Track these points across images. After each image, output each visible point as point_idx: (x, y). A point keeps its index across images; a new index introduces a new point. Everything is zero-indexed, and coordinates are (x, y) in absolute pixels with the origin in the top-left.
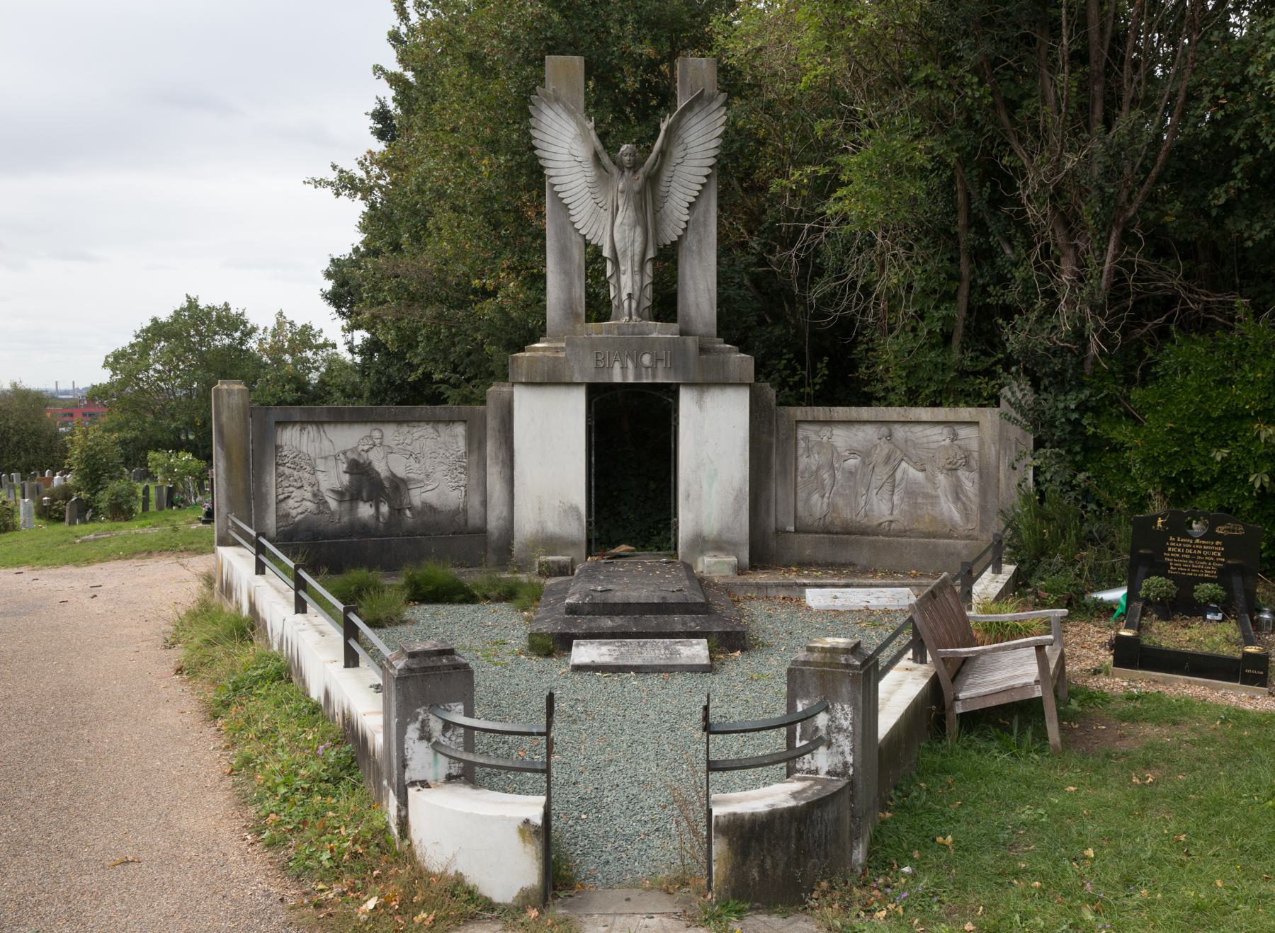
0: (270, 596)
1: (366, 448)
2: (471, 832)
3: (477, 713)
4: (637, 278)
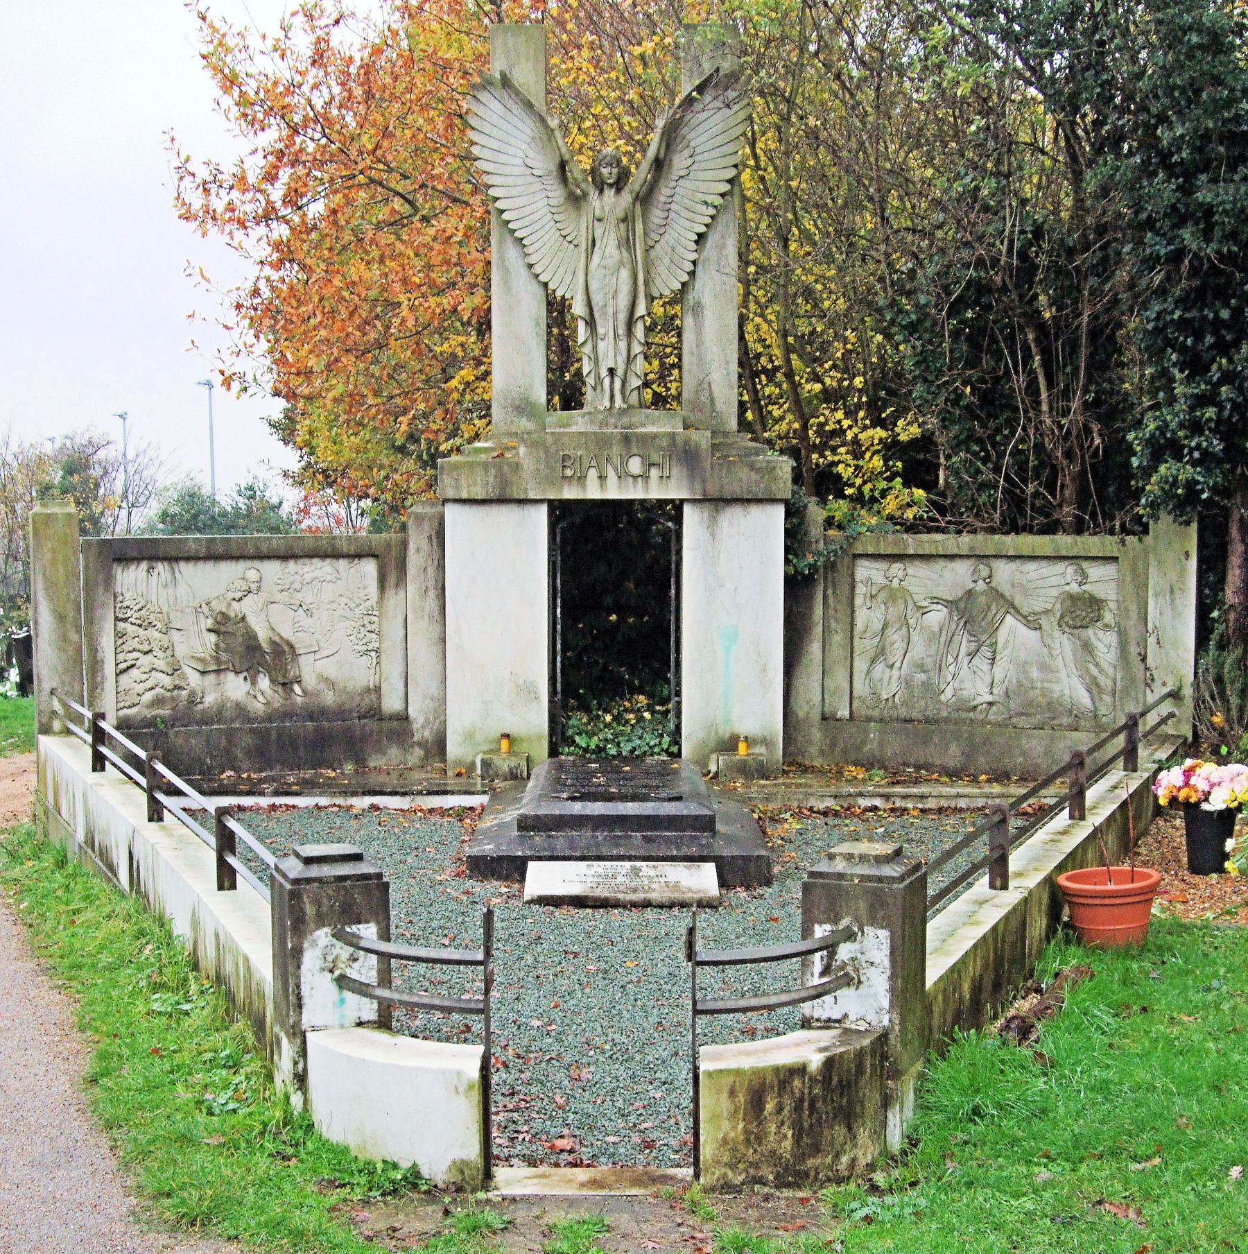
0: (111, 803)
1: (238, 595)
2: (393, 1093)
3: (397, 982)
4: (623, 345)
